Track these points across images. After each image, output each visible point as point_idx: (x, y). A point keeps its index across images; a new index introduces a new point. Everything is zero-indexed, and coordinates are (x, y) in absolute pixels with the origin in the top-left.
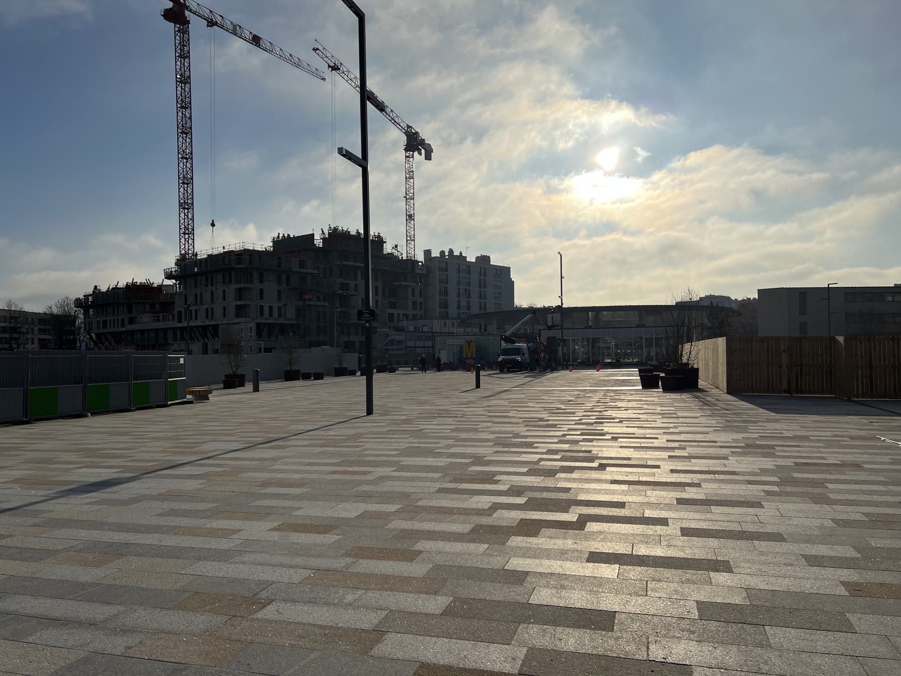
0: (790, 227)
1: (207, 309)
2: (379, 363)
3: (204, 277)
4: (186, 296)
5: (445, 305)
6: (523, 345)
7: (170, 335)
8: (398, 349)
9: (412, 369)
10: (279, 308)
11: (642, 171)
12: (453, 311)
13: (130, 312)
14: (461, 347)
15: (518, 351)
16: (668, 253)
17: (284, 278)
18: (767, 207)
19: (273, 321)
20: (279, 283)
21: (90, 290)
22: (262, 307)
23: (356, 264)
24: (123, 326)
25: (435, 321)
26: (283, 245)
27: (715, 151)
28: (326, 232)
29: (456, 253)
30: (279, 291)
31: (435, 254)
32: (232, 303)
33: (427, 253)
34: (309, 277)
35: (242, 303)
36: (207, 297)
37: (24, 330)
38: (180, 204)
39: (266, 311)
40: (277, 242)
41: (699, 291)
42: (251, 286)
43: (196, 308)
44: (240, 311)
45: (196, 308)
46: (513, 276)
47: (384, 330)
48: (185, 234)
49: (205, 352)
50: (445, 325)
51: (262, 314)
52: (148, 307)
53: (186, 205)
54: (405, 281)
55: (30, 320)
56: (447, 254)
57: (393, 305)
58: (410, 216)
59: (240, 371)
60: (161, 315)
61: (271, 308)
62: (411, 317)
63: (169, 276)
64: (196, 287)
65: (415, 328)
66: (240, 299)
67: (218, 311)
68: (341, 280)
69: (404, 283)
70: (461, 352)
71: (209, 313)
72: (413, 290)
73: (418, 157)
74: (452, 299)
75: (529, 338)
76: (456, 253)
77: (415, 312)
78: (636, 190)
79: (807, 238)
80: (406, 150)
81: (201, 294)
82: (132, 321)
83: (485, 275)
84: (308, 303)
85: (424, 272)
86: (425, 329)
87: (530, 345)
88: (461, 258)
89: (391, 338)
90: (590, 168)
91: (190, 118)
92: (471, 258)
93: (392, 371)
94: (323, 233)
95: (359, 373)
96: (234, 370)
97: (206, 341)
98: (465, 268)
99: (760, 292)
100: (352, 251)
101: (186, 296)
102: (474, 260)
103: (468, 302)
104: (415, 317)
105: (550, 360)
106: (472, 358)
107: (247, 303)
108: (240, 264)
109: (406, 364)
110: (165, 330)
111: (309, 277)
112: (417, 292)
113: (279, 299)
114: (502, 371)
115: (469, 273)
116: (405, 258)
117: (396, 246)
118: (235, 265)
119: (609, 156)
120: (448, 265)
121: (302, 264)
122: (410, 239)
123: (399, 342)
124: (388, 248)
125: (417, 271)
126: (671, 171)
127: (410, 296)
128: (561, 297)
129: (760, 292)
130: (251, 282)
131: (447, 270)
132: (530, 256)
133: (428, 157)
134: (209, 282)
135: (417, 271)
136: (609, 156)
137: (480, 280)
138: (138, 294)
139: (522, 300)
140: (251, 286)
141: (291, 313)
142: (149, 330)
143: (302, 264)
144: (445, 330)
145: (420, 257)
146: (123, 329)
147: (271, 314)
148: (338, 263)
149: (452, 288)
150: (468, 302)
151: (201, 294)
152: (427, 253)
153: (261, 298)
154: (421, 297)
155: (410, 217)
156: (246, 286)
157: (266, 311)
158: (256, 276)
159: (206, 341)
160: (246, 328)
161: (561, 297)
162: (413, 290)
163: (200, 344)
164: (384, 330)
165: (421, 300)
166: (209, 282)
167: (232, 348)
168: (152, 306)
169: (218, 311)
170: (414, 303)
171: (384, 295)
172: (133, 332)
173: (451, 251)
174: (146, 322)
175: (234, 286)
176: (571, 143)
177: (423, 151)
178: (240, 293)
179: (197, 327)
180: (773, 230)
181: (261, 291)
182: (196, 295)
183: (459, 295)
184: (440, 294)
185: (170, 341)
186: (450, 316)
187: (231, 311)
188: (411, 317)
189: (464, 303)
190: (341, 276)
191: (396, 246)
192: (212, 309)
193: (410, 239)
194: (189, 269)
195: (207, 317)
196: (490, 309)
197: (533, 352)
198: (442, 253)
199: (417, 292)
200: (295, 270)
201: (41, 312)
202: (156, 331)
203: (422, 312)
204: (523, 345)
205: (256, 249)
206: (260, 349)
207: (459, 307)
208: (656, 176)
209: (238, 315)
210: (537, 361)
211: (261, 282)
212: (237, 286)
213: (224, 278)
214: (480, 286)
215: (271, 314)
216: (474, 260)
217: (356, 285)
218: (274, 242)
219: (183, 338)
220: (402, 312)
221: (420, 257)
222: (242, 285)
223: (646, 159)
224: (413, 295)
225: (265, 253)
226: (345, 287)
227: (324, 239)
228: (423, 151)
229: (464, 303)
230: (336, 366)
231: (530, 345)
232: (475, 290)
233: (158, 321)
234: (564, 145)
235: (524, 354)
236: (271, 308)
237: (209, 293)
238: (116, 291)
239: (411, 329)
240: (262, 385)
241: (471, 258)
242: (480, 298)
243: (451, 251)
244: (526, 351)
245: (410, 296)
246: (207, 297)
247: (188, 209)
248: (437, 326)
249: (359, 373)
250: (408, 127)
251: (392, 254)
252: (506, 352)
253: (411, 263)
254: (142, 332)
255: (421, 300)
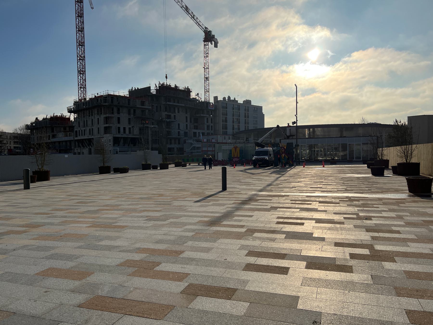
0: (407, 90)
1: (90, 129)
2: (177, 161)
3: (88, 111)
4: (79, 122)
5: (225, 127)
6: (270, 149)
7: (73, 144)
8: (197, 152)
9: (199, 165)
10: (130, 128)
11: (331, 61)
12: (230, 131)
13: (53, 131)
14: (231, 151)
15: (266, 153)
16: (344, 104)
17: (132, 111)
18: (395, 79)
19: (126, 136)
20: (129, 114)
21: (33, 120)
22: (119, 128)
23: (174, 104)
24: (49, 139)
25: (219, 136)
26: (134, 93)
27: (370, 51)
28: (158, 86)
29: (232, 98)
30: (129, 119)
31: (220, 98)
32: (102, 126)
33: (216, 98)
34: (147, 111)
35: (107, 125)
36: (90, 123)
37: (5, 142)
38: (78, 71)
39: (122, 130)
40: (131, 92)
41: (370, 119)
42: (112, 116)
43: (84, 129)
44: (107, 130)
45: (84, 129)
46: (264, 111)
47: (190, 141)
48: (81, 88)
49: (90, 153)
50: (225, 138)
51: (119, 132)
52: (62, 129)
53: (82, 72)
54: (203, 114)
55: (9, 137)
56: (227, 99)
57: (196, 128)
58: (207, 78)
59: (46, 168)
60: (68, 133)
61: (124, 129)
62: (206, 134)
63: (70, 111)
64: (84, 117)
65: (207, 140)
66: (107, 123)
67: (95, 131)
68: (166, 113)
69: (202, 115)
70: (231, 153)
71: (91, 132)
72: (207, 119)
73: (211, 46)
74: (230, 124)
75: (273, 145)
76: (232, 98)
77: (208, 131)
78: (327, 72)
79: (416, 95)
80: (205, 41)
81: (87, 121)
82: (54, 136)
83: (248, 111)
84: (145, 125)
85: (213, 109)
86: (213, 141)
87: (274, 149)
88: (235, 101)
89: (193, 146)
90: (304, 60)
91: (83, 22)
92: (241, 101)
93: (185, 166)
94: (156, 86)
95: (159, 168)
96: (40, 167)
97: (91, 147)
98: (236, 106)
99: (410, 118)
100: (171, 97)
101: (79, 122)
102: (242, 103)
103: (239, 126)
104: (208, 134)
105: (288, 159)
106: (237, 157)
107: (111, 125)
108: (106, 103)
109: (193, 161)
110: (70, 141)
111: (147, 111)
112: (210, 120)
113: (129, 123)
114: (255, 167)
115: (239, 110)
116: (203, 100)
117: (198, 94)
118: (106, 104)
119: (314, 54)
120: (228, 104)
121: (143, 103)
122: (207, 91)
123: (198, 148)
124: (193, 95)
125: (209, 108)
126: (345, 62)
127: (206, 123)
128: (296, 116)
129: (410, 118)
130: (113, 113)
131: (227, 108)
132: (273, 106)
133: (216, 46)
134: (91, 114)
135: (209, 108)
136: (314, 54)
137: (245, 113)
138: (57, 122)
139: (269, 123)
140: (112, 116)
141: (136, 131)
142: (62, 141)
143: (143, 103)
144: (224, 141)
145: (212, 101)
146: (49, 141)
147: (125, 132)
148: (164, 103)
149: (230, 118)
150: (239, 126)
151: (87, 121)
152: (216, 98)
153: (119, 122)
154: (212, 123)
155: (207, 79)
156: (110, 115)
157: (122, 130)
158: (115, 110)
159: (91, 147)
160: (108, 139)
161: (296, 116)
162: (207, 119)
163: (87, 149)
164: (190, 141)
165: (212, 125)
166: (91, 114)
167: (101, 151)
168: (65, 128)
169: (95, 131)
170: (208, 127)
171: (191, 122)
172: (55, 142)
173: (229, 97)
174: (61, 137)
175: (103, 116)
176: (295, 49)
177: (213, 42)
178: (107, 120)
179: (85, 139)
180: (399, 91)
181: (119, 119)
182: (84, 121)
183: (233, 122)
184: (223, 121)
185: (73, 148)
186: (228, 133)
187: (102, 130)
188: (206, 134)
189: (236, 127)
190: (166, 111)
191: (198, 94)
192: (92, 129)
193: (207, 91)
194: (80, 107)
195: (90, 134)
196: (251, 127)
197: (276, 153)
198: (224, 98)
199: (210, 120)
200: (138, 106)
201: (12, 132)
202: (66, 142)
203: (212, 132)
204: (270, 149)
205: (115, 94)
206: (117, 152)
207: (233, 129)
208: (337, 66)
209: (105, 133)
210: (279, 160)
211: (119, 113)
212: (105, 116)
213: (98, 112)
214: (245, 117)
215: (125, 132)
216: (242, 103)
217: (175, 116)
218: (129, 92)
219: (79, 146)
220: (201, 131)
221: (212, 101)
222: (107, 115)
223: (332, 56)
224: (207, 122)
225: (124, 97)
226: (169, 117)
227: (156, 90)
228: (213, 42)
229: (236, 127)
230: (143, 163)
231: (274, 149)
232: (242, 119)
233: (67, 136)
234: (292, 50)
235: (270, 155)
236: (124, 129)
237: (91, 120)
238: (45, 120)
239: (205, 140)
240: (32, 185)
241: (241, 101)
242: (245, 123)
243: (229, 97)
244: (272, 153)
245: (206, 123)
246: (90, 123)
247: (83, 74)
248: (220, 138)
249: (159, 168)
250: (206, 28)
251: (195, 99)
252: (258, 153)
253: (207, 103)
254: (59, 142)
255: (212, 125)
